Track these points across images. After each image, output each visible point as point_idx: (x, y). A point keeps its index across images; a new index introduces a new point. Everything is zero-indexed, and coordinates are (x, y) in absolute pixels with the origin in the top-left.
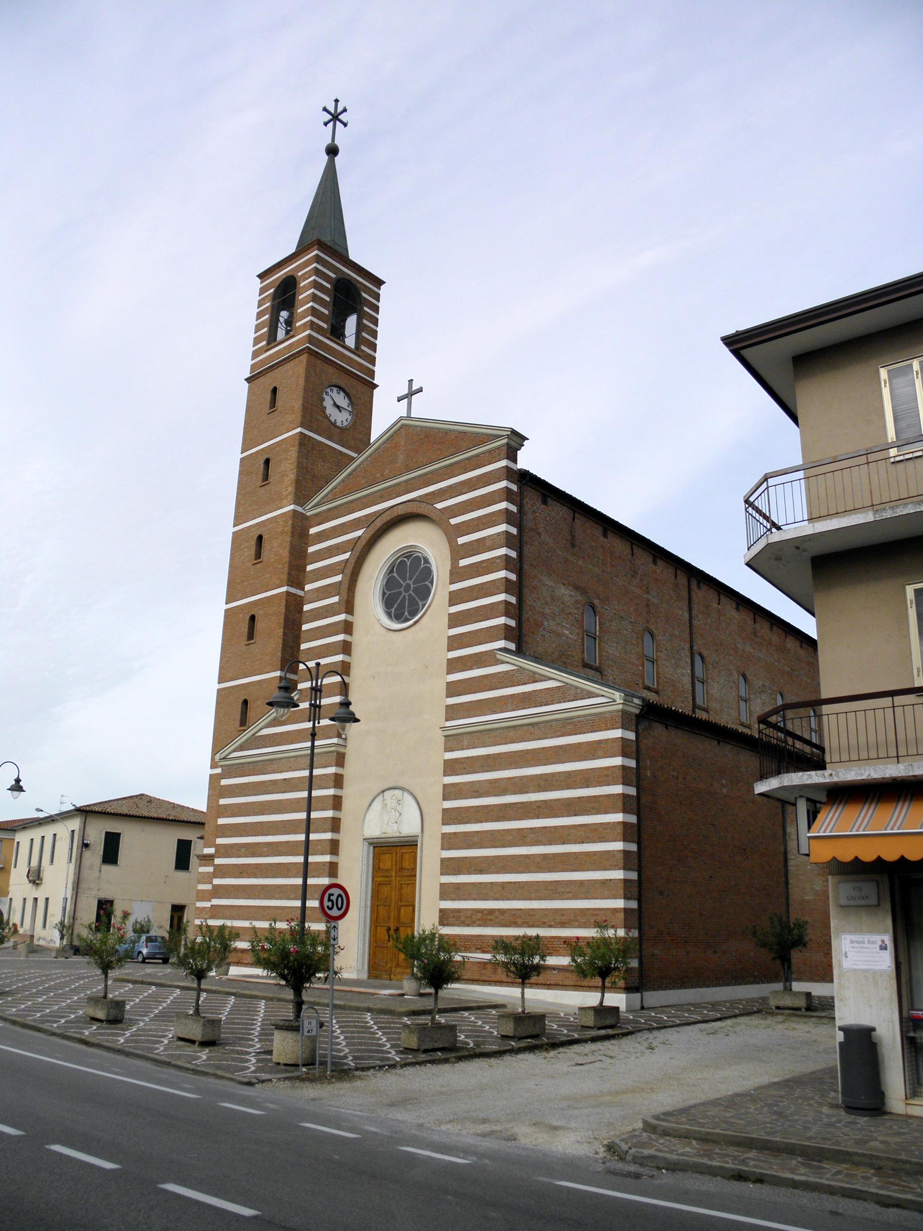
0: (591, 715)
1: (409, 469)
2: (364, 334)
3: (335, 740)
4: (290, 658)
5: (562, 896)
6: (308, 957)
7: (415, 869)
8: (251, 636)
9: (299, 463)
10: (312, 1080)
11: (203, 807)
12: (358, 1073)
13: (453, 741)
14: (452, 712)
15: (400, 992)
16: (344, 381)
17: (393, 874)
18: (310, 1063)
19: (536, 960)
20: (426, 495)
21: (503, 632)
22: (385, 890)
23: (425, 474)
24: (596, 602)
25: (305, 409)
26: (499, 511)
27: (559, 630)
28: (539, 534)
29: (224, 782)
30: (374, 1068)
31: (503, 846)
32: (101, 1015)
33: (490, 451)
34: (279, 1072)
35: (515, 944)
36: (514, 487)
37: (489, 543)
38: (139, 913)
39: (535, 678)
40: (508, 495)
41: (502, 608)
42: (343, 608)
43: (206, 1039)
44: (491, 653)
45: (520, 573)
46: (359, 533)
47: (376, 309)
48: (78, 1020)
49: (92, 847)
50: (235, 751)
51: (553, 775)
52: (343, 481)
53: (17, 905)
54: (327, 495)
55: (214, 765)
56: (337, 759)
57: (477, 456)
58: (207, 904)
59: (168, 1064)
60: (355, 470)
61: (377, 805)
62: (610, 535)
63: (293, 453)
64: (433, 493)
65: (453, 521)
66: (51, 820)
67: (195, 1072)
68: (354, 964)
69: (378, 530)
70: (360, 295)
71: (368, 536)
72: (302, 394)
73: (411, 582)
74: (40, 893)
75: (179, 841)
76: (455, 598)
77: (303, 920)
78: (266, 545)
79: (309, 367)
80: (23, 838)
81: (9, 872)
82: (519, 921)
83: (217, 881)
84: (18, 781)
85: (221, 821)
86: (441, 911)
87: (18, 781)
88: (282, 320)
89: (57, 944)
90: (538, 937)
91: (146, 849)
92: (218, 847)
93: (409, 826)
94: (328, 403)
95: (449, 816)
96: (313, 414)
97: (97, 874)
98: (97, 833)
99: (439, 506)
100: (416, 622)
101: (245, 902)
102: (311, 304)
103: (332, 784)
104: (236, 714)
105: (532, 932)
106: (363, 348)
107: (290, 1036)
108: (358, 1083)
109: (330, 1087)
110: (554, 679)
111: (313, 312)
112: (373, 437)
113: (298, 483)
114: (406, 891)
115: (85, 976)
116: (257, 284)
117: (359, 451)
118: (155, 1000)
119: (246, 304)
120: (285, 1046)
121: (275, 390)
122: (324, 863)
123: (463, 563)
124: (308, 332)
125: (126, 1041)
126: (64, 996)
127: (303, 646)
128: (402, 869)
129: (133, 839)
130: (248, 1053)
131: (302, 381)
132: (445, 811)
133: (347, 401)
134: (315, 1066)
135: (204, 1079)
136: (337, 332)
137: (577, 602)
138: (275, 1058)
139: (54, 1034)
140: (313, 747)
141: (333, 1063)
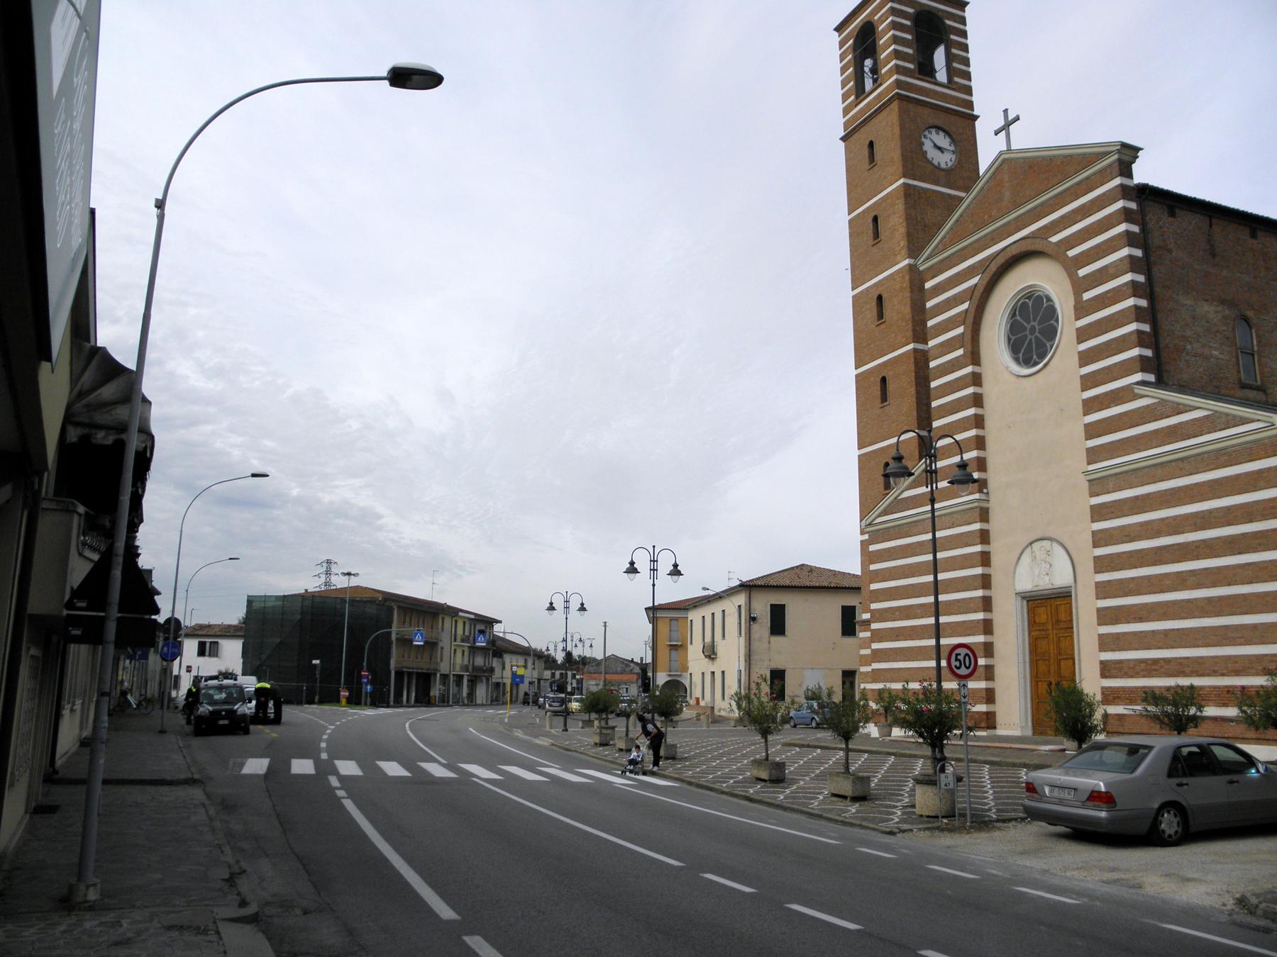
0: (1247, 443)
1: (1017, 206)
2: (955, 65)
3: (977, 496)
4: (924, 417)
5: (1233, 642)
6: (941, 714)
7: (1071, 621)
8: (884, 398)
9: (907, 215)
10: (951, 830)
11: (859, 572)
12: (998, 824)
13: (1097, 485)
14: (1094, 455)
15: (1061, 747)
16: (941, 120)
17: (1050, 627)
18: (950, 815)
19: (1193, 711)
20: (1039, 229)
21: (1138, 364)
22: (1043, 644)
23: (1035, 208)
24: (1250, 314)
25: (905, 158)
26: (1119, 234)
27: (1206, 351)
28: (1170, 251)
29: (872, 548)
30: (1015, 819)
31: (1162, 591)
32: (764, 775)
33: (1100, 171)
34: (921, 823)
35: (1166, 694)
36: (1133, 205)
37: (1111, 271)
38: (813, 679)
39: (1180, 409)
40: (1127, 215)
41: (1134, 338)
42: (969, 360)
43: (856, 794)
44: (1128, 388)
45: (1151, 298)
46: (975, 280)
47: (964, 34)
48: (745, 781)
49: (759, 621)
50: (879, 516)
51: (1210, 512)
52: (951, 229)
53: (697, 679)
54: (937, 246)
55: (862, 533)
56: (981, 515)
57: (1088, 178)
58: (868, 669)
59: (820, 817)
60: (961, 215)
61: (1026, 558)
62: (1260, 234)
63: (900, 206)
64: (1045, 227)
65: (1071, 253)
66: (718, 597)
67: (844, 823)
68: (1017, 721)
69: (995, 274)
70: (944, 24)
71: (985, 282)
72: (899, 143)
73: (1035, 324)
74: (717, 667)
75: (843, 607)
76: (1082, 335)
77: (939, 681)
78: (886, 303)
79: (902, 113)
80: (695, 616)
81: (686, 649)
82: (1187, 670)
83: (875, 646)
84: (676, 566)
85: (874, 586)
86: (1102, 662)
87: (676, 566)
88: (866, 69)
89: (736, 714)
90: (1192, 687)
91: (813, 619)
92: (873, 612)
93: (1061, 576)
94: (928, 146)
95: (1102, 564)
96: (914, 162)
97: (766, 645)
98: (762, 606)
99: (1054, 239)
100: (1045, 365)
101: (895, 663)
102: (893, 47)
103: (978, 540)
104: (883, 474)
105: (1185, 682)
106: (956, 79)
107: (929, 790)
108: (996, 834)
109: (967, 837)
110: (1201, 408)
111: (897, 54)
112: (981, 172)
113: (909, 236)
114: (1064, 644)
115: (752, 743)
116: (836, 38)
117: (967, 189)
118: (819, 761)
119: (828, 59)
120: (926, 800)
121: (871, 144)
122: (978, 621)
123: (1087, 296)
124: (895, 77)
125: (786, 798)
126: (736, 760)
127: (934, 404)
128: (1058, 621)
129: (796, 608)
130: (895, 807)
131: (897, 130)
132: (1097, 559)
133: (948, 139)
134: (955, 817)
135: (850, 829)
136: (927, 70)
137: (1225, 318)
138: (918, 811)
139: (723, 793)
140: (933, 510)
141: (973, 816)
